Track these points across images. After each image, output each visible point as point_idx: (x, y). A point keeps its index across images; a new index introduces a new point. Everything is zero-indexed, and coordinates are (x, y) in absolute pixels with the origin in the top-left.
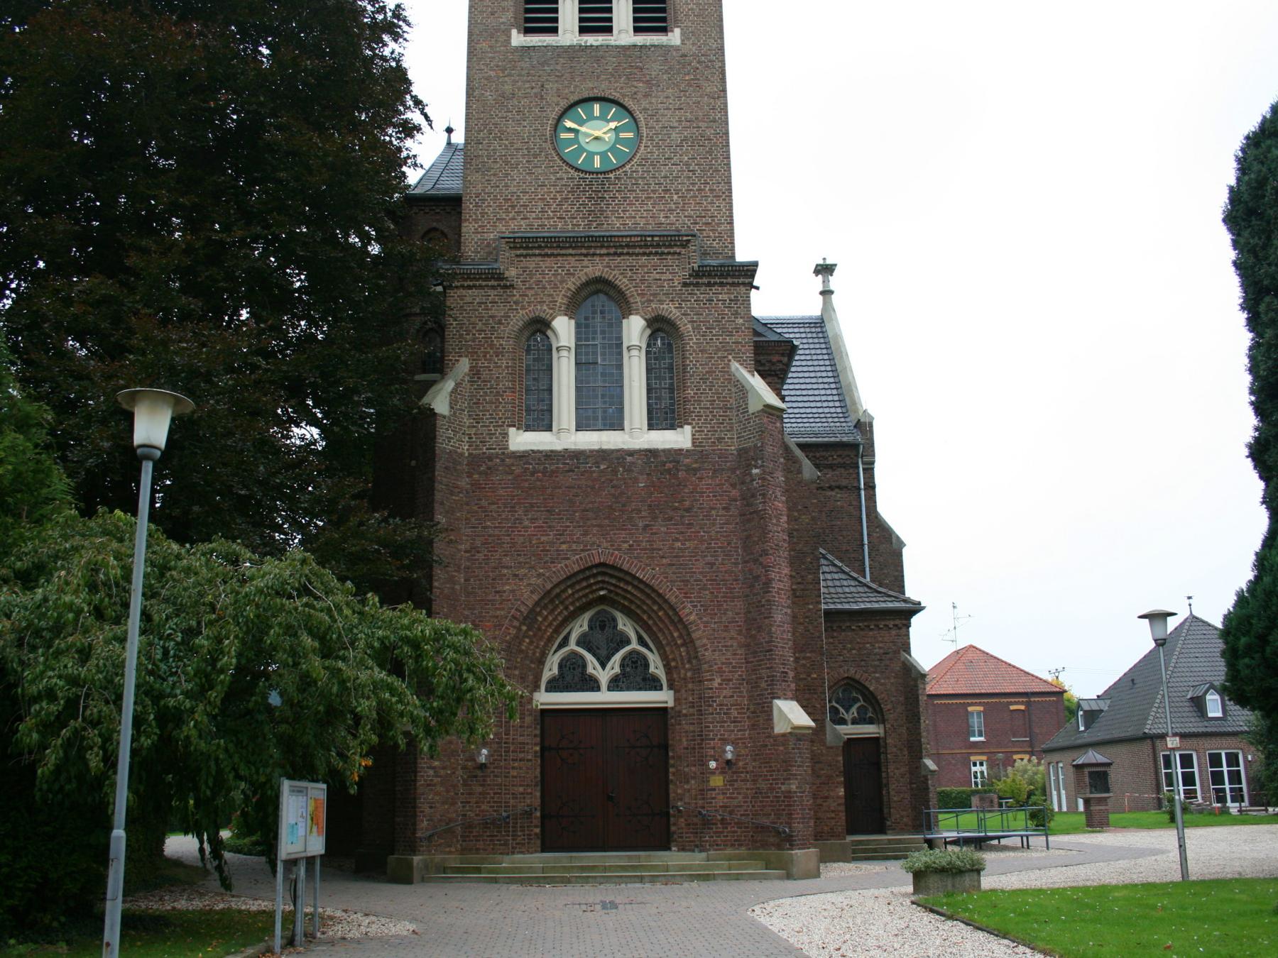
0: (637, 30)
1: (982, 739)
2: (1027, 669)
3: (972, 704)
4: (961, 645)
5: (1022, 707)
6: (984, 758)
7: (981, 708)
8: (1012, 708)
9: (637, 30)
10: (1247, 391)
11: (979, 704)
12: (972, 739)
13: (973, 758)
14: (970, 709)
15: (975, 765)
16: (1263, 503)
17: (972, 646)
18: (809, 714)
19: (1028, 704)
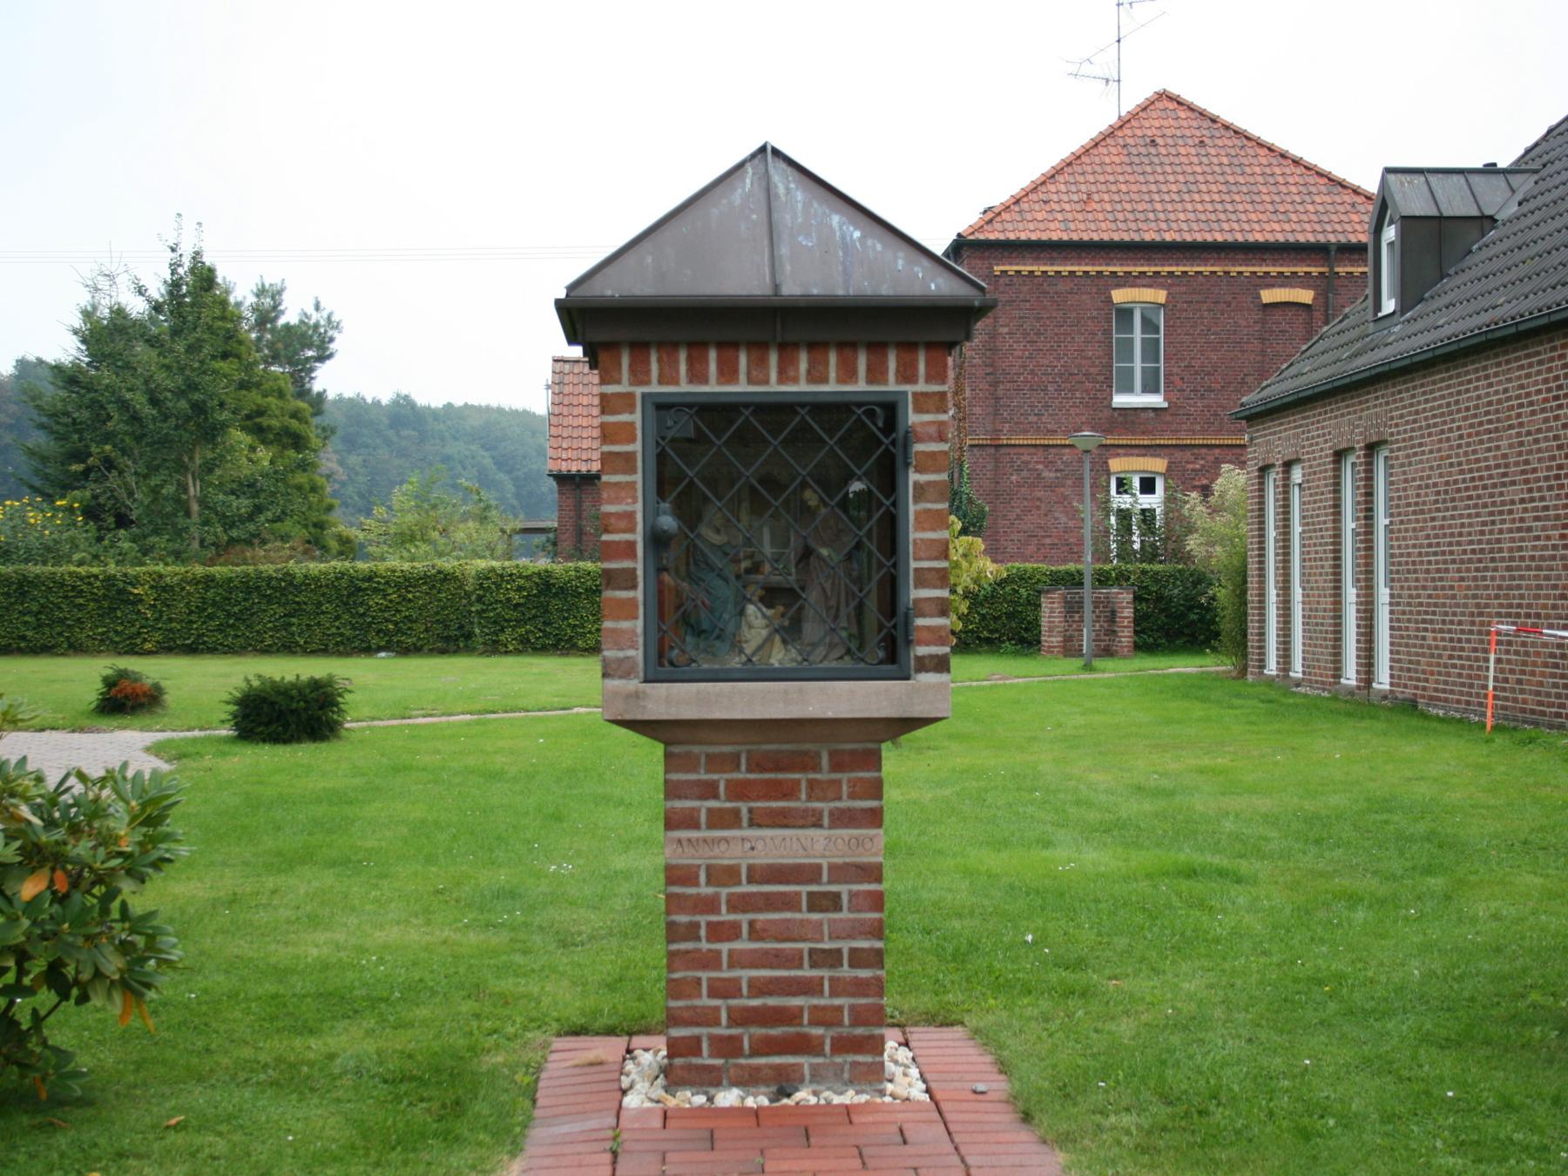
0: (890, 409)
1: (1156, 400)
2: (1339, 172)
3: (1127, 280)
4: (1133, 98)
5: (1305, 296)
6: (1157, 464)
7: (1161, 296)
8: (1268, 296)
9: (890, 409)
10: (596, 219)
11: (1154, 280)
12: (1120, 400)
13: (1116, 464)
14: (1119, 296)
15: (1122, 486)
16: (196, 291)
17: (1164, 95)
18: (76, 649)
19: (1326, 286)
